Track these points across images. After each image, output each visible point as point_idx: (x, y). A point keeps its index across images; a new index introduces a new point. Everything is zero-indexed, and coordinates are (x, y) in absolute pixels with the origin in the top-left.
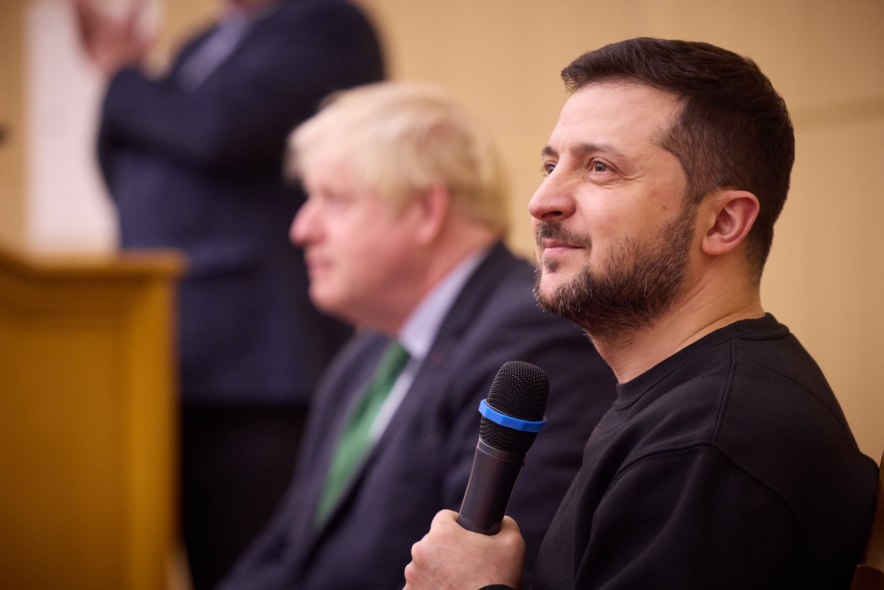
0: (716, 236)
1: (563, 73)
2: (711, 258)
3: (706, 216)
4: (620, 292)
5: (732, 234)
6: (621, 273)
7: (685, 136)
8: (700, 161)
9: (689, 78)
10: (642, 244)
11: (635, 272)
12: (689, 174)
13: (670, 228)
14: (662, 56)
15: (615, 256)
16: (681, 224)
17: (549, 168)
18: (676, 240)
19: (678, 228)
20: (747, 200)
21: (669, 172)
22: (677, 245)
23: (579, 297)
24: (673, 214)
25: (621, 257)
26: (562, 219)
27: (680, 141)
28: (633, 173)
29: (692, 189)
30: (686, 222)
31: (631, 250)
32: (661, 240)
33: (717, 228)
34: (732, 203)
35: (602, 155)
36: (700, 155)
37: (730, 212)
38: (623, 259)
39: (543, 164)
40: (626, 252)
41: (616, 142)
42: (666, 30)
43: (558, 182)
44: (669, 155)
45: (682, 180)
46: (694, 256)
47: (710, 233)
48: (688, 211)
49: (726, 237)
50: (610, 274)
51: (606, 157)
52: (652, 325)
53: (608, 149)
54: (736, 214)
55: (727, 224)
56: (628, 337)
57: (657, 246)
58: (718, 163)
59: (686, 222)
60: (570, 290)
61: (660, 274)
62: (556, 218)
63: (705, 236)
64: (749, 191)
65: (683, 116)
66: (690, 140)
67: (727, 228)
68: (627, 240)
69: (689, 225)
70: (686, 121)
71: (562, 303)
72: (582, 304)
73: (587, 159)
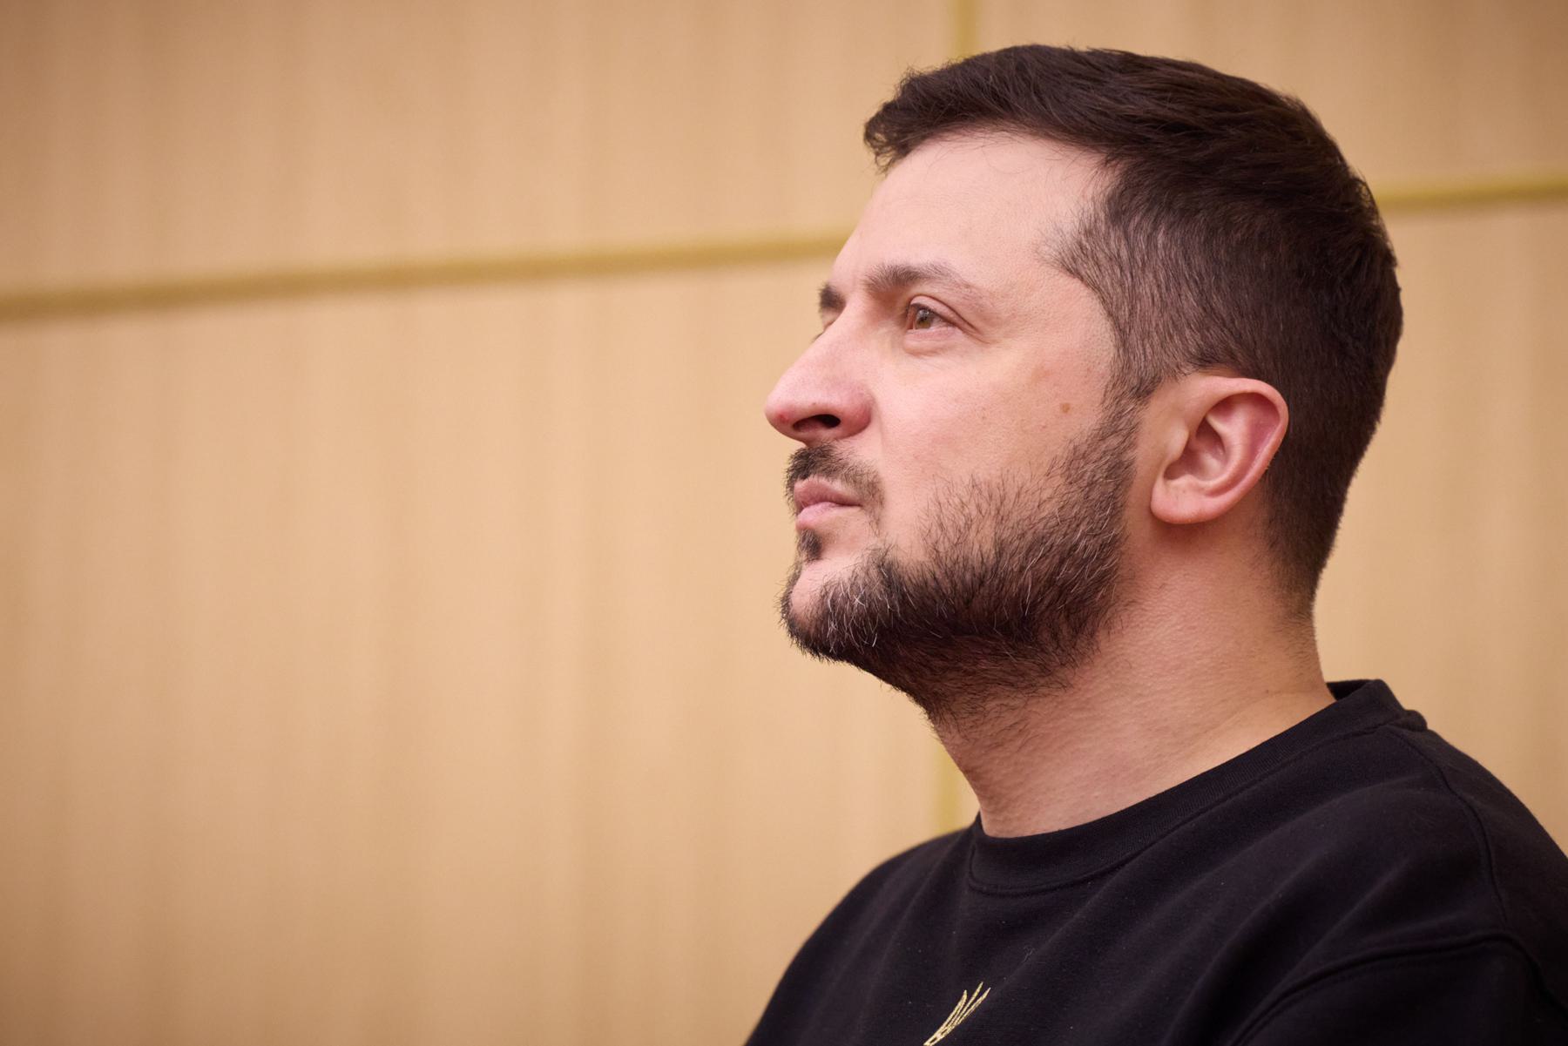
0: (1184, 481)
1: (871, 129)
2: (1183, 535)
5: (1224, 477)
6: (966, 559)
7: (1113, 245)
8: (1147, 301)
11: (999, 554)
12: (1122, 332)
13: (1078, 457)
15: (947, 523)
16: (1103, 447)
18: (1091, 484)
19: (1095, 456)
20: (1257, 399)
21: (1069, 333)
22: (1095, 495)
24: (1087, 419)
25: (962, 523)
27: (1101, 256)
29: (1127, 366)
30: (1113, 442)
31: (985, 506)
32: (1058, 481)
34: (1225, 405)
36: (1146, 288)
37: (1219, 425)
38: (968, 526)
40: (974, 513)
44: (1075, 284)
47: (1170, 474)
48: (1119, 416)
49: (1213, 483)
50: (938, 560)
52: (1065, 686)
53: (937, 273)
54: (1234, 429)
55: (1215, 455)
57: (1041, 496)
58: (1190, 302)
59: (1113, 442)
60: (847, 598)
61: (1062, 562)
62: (825, 434)
63: (1160, 482)
64: (1269, 381)
65: (1110, 200)
66: (1124, 254)
67: (1210, 461)
70: (1118, 210)
71: (832, 627)
73: (903, 302)
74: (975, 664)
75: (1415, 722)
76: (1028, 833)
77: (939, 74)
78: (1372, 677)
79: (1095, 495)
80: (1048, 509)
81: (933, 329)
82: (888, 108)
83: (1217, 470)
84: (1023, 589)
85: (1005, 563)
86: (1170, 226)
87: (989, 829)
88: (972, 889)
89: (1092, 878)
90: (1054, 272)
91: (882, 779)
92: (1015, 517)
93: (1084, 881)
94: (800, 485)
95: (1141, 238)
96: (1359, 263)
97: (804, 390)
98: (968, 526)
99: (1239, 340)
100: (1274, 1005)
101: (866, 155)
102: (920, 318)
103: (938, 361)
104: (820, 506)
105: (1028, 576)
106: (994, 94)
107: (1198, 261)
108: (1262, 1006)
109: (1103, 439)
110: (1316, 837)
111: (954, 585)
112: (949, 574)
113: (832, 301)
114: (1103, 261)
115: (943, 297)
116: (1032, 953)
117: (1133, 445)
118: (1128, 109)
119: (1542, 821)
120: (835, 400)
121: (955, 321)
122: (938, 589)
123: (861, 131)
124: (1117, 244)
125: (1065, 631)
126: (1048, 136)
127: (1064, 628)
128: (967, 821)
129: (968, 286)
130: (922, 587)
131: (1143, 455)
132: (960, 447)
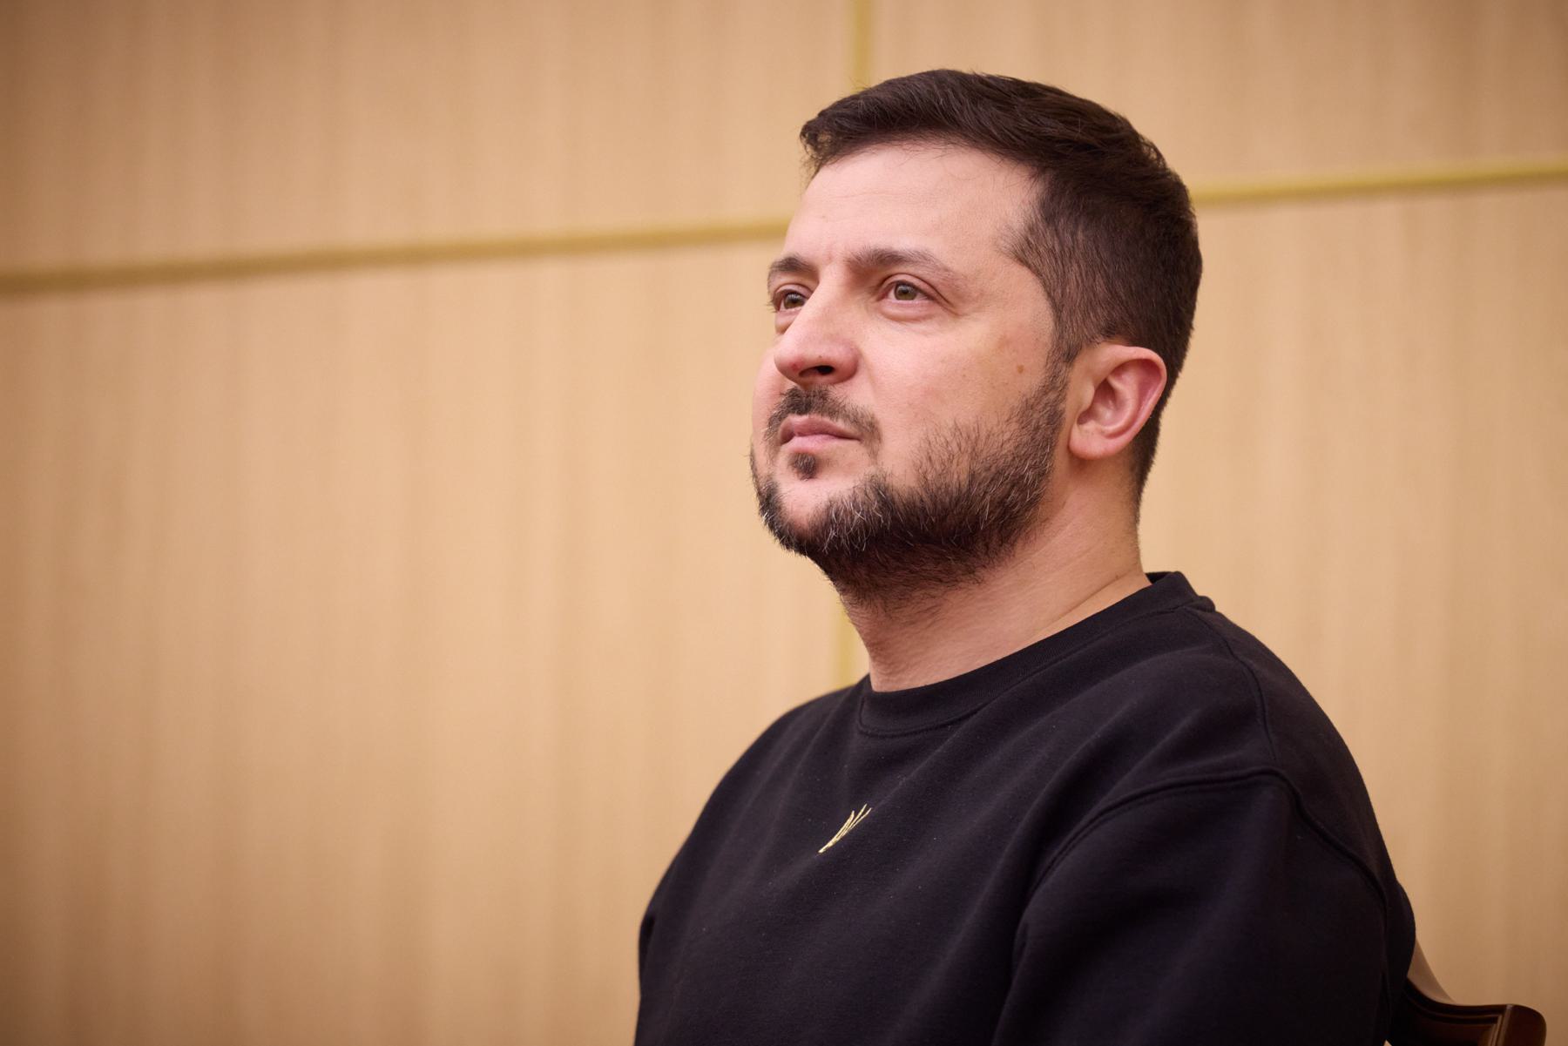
0: (1091, 426)
1: (810, 133)
2: (1081, 464)
4: (944, 519)
5: (1120, 424)
8: (1073, 284)
9: (1050, 139)
10: (983, 434)
11: (971, 484)
12: (1057, 308)
13: (1029, 406)
14: (995, 100)
16: (1045, 400)
17: (789, 300)
18: (1037, 428)
20: (1146, 364)
21: (1018, 310)
24: (1033, 380)
25: (945, 457)
26: (833, 383)
29: (1061, 337)
32: (1014, 426)
34: (1120, 368)
35: (911, 269)
36: (1073, 274)
39: (768, 298)
40: (956, 450)
41: (937, 247)
43: (826, 316)
44: (1024, 273)
45: (1047, 322)
46: (1060, 462)
50: (926, 486)
51: (920, 272)
52: (979, 582)
53: (923, 258)
54: (1126, 386)
56: (929, 603)
57: (1003, 437)
58: (1100, 287)
59: (1052, 396)
62: (822, 380)
66: (1057, 248)
67: (1106, 413)
68: (956, 428)
69: (1057, 401)
70: (1049, 212)
73: (879, 276)
75: (1207, 605)
78: (1172, 569)
79: (1038, 437)
80: (1009, 447)
81: (917, 301)
87: (877, 685)
88: (861, 733)
89: (952, 723)
90: (1008, 261)
91: (806, 644)
92: (984, 454)
93: (944, 726)
100: (1092, 821)
101: (799, 151)
103: (921, 327)
104: (819, 438)
108: (1083, 823)
109: (1046, 393)
110: (1122, 695)
111: (935, 504)
112: (934, 498)
115: (927, 278)
116: (903, 780)
119: (1305, 684)
120: (832, 353)
122: (923, 509)
123: (800, 131)
124: (1050, 241)
126: (983, 150)
127: (995, 538)
128: (854, 679)
129: (947, 270)
130: (910, 506)
131: (1070, 408)
132: (927, 392)
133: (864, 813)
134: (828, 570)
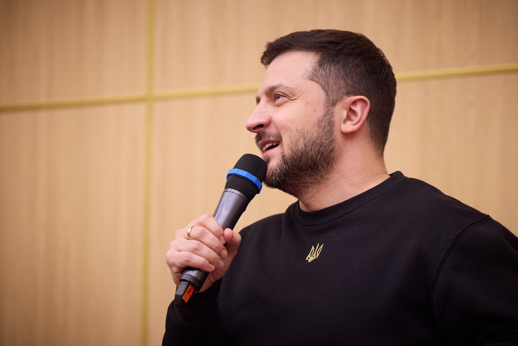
0: (349, 123)
1: (263, 59)
2: (349, 136)
3: (340, 112)
4: (301, 160)
8: (332, 84)
10: (306, 131)
11: (305, 147)
12: (326, 92)
13: (320, 121)
15: (293, 141)
18: (324, 127)
21: (316, 93)
22: (326, 130)
23: (282, 171)
24: (320, 113)
27: (318, 75)
28: (295, 96)
29: (329, 99)
32: (316, 128)
33: (348, 118)
34: (354, 103)
36: (331, 81)
37: (353, 108)
38: (298, 141)
42: (307, 26)
44: (313, 83)
45: (322, 95)
46: (338, 137)
47: (345, 122)
49: (354, 122)
50: (292, 151)
54: (358, 108)
55: (355, 116)
58: (342, 82)
59: (328, 117)
61: (320, 147)
62: (261, 129)
63: (342, 124)
66: (324, 73)
67: (353, 117)
70: (321, 64)
72: (284, 175)
73: (274, 95)
74: (306, 179)
76: (322, 208)
77: (274, 43)
79: (326, 130)
80: (315, 134)
82: (265, 53)
83: (356, 119)
84: (312, 155)
85: (307, 149)
86: (334, 65)
92: (307, 137)
94: (260, 142)
95: (328, 69)
96: (382, 68)
97: (255, 121)
98: (298, 141)
99: (356, 88)
102: (277, 97)
105: (313, 152)
106: (287, 43)
107: (342, 72)
113: (258, 100)
114: (319, 76)
115: (282, 91)
117: (333, 117)
118: (320, 40)
121: (285, 95)
123: (260, 61)
125: (325, 165)
126: (304, 50)
133: (310, 258)
134: (280, 189)
